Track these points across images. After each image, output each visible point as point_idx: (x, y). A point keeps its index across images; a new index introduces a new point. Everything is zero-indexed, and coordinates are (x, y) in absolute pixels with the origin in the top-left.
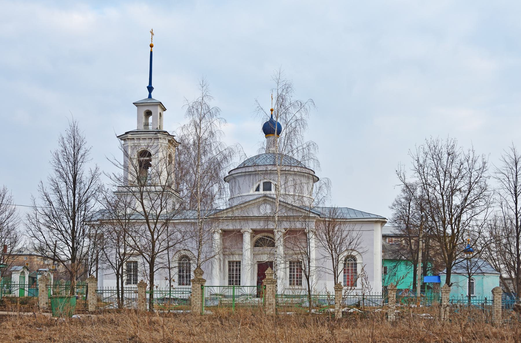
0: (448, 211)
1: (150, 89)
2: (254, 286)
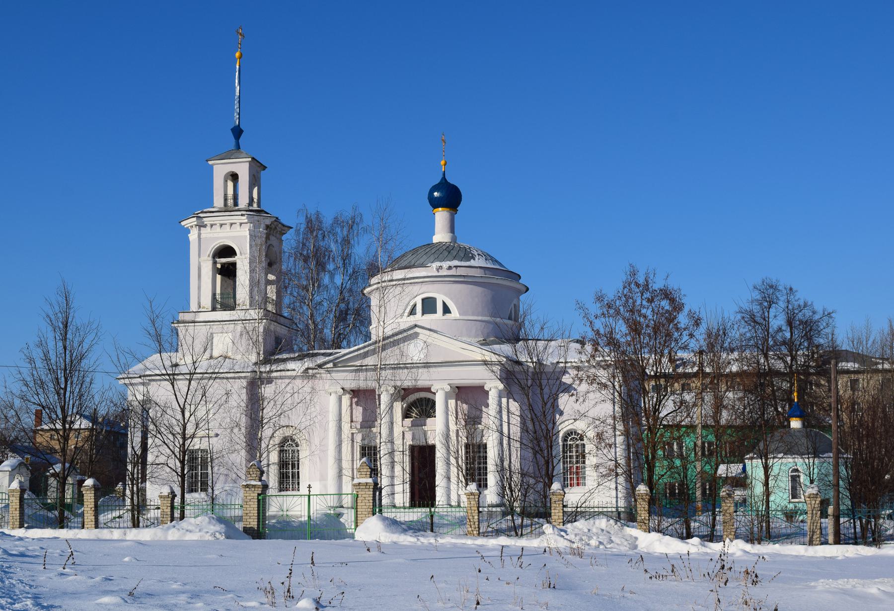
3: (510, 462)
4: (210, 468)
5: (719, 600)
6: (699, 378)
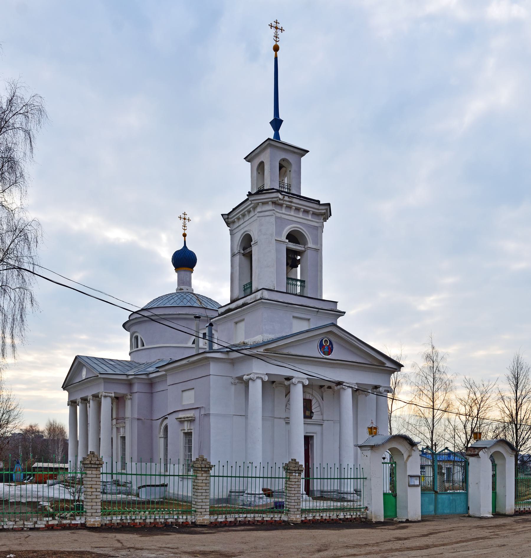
0: (430, 484)
1: (277, 123)
2: (116, 474)
3: (527, 527)
4: (293, 204)
5: (116, 463)
6: (49, 514)
